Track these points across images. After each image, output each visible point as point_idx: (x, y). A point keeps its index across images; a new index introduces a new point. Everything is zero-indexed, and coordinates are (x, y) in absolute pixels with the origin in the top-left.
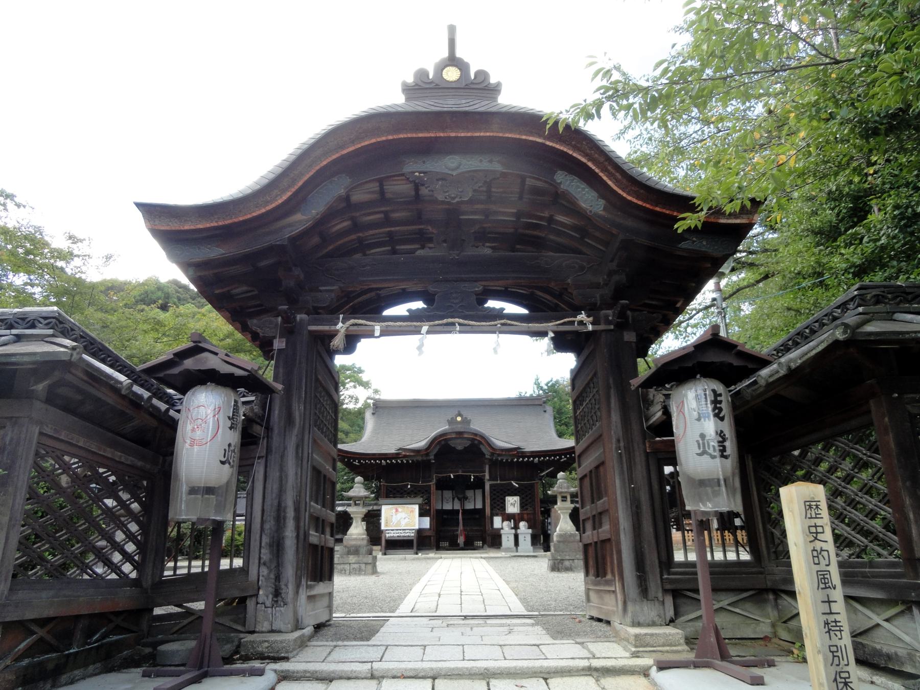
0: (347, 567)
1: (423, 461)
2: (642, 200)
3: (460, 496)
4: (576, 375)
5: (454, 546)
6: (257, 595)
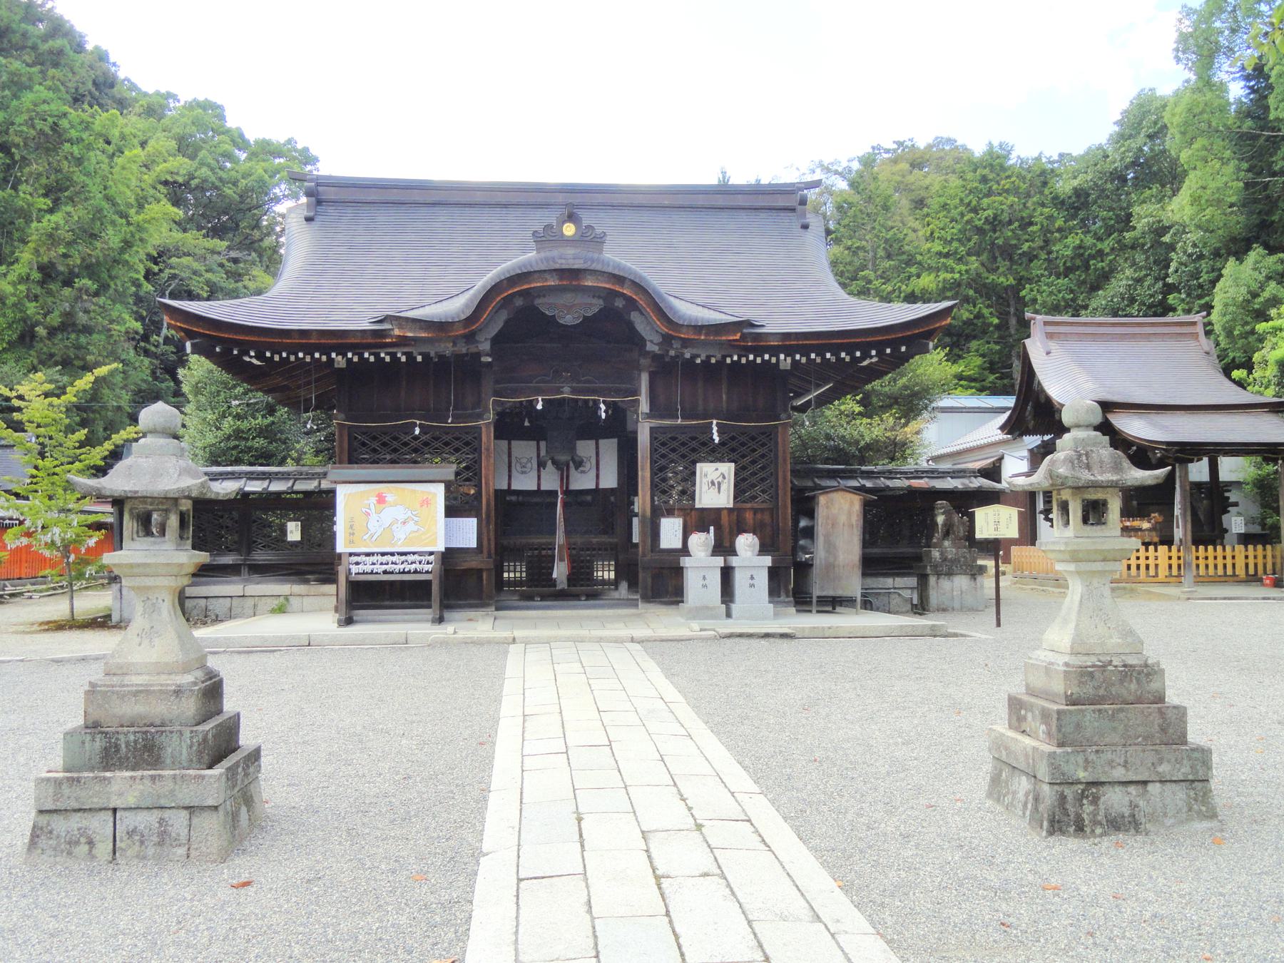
0: (100, 825)
1: (459, 357)
3: (563, 458)
5: (540, 590)
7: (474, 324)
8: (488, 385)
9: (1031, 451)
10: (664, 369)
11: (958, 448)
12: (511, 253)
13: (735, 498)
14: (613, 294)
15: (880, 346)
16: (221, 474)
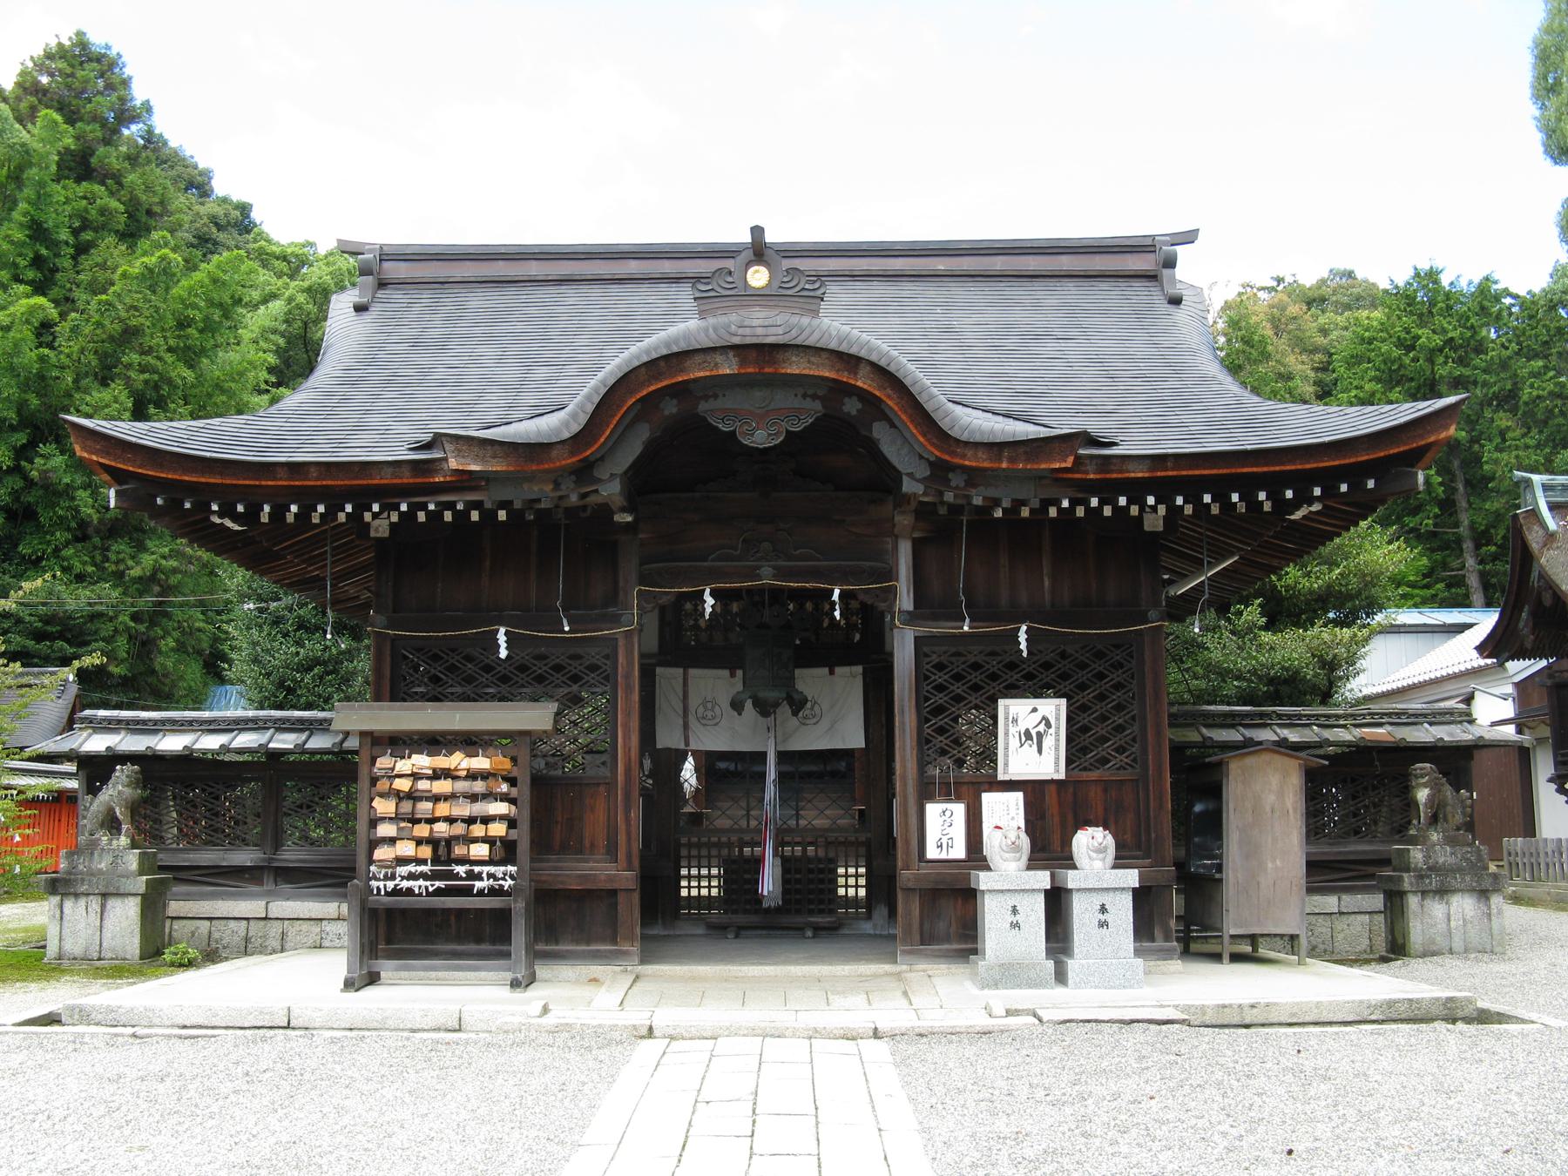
7: (589, 445)
8: (629, 567)
9: (1517, 685)
10: (940, 530)
11: (1389, 687)
13: (1069, 762)
14: (842, 390)
15: (1329, 478)
16: (163, 722)
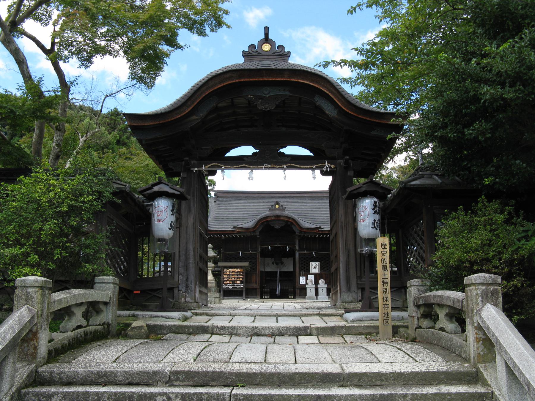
2: (353, 112)
4: (332, 186)
6: (178, 287)
10: (302, 239)
12: (263, 211)
